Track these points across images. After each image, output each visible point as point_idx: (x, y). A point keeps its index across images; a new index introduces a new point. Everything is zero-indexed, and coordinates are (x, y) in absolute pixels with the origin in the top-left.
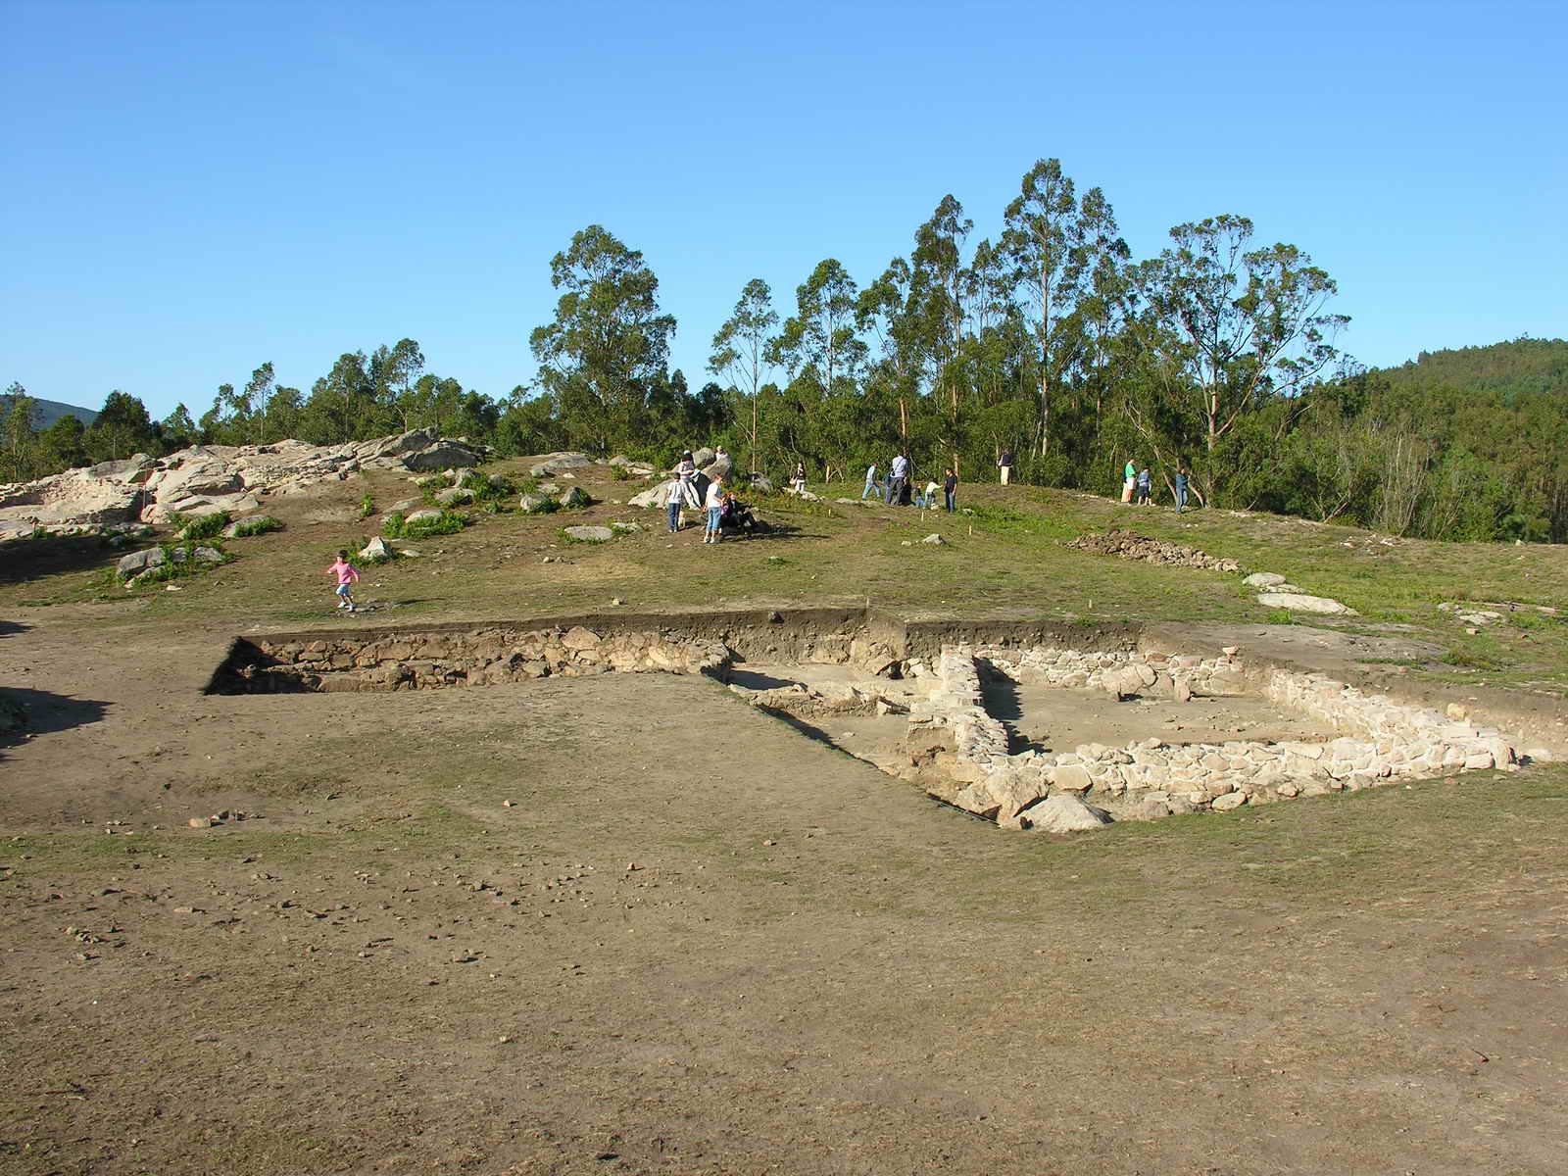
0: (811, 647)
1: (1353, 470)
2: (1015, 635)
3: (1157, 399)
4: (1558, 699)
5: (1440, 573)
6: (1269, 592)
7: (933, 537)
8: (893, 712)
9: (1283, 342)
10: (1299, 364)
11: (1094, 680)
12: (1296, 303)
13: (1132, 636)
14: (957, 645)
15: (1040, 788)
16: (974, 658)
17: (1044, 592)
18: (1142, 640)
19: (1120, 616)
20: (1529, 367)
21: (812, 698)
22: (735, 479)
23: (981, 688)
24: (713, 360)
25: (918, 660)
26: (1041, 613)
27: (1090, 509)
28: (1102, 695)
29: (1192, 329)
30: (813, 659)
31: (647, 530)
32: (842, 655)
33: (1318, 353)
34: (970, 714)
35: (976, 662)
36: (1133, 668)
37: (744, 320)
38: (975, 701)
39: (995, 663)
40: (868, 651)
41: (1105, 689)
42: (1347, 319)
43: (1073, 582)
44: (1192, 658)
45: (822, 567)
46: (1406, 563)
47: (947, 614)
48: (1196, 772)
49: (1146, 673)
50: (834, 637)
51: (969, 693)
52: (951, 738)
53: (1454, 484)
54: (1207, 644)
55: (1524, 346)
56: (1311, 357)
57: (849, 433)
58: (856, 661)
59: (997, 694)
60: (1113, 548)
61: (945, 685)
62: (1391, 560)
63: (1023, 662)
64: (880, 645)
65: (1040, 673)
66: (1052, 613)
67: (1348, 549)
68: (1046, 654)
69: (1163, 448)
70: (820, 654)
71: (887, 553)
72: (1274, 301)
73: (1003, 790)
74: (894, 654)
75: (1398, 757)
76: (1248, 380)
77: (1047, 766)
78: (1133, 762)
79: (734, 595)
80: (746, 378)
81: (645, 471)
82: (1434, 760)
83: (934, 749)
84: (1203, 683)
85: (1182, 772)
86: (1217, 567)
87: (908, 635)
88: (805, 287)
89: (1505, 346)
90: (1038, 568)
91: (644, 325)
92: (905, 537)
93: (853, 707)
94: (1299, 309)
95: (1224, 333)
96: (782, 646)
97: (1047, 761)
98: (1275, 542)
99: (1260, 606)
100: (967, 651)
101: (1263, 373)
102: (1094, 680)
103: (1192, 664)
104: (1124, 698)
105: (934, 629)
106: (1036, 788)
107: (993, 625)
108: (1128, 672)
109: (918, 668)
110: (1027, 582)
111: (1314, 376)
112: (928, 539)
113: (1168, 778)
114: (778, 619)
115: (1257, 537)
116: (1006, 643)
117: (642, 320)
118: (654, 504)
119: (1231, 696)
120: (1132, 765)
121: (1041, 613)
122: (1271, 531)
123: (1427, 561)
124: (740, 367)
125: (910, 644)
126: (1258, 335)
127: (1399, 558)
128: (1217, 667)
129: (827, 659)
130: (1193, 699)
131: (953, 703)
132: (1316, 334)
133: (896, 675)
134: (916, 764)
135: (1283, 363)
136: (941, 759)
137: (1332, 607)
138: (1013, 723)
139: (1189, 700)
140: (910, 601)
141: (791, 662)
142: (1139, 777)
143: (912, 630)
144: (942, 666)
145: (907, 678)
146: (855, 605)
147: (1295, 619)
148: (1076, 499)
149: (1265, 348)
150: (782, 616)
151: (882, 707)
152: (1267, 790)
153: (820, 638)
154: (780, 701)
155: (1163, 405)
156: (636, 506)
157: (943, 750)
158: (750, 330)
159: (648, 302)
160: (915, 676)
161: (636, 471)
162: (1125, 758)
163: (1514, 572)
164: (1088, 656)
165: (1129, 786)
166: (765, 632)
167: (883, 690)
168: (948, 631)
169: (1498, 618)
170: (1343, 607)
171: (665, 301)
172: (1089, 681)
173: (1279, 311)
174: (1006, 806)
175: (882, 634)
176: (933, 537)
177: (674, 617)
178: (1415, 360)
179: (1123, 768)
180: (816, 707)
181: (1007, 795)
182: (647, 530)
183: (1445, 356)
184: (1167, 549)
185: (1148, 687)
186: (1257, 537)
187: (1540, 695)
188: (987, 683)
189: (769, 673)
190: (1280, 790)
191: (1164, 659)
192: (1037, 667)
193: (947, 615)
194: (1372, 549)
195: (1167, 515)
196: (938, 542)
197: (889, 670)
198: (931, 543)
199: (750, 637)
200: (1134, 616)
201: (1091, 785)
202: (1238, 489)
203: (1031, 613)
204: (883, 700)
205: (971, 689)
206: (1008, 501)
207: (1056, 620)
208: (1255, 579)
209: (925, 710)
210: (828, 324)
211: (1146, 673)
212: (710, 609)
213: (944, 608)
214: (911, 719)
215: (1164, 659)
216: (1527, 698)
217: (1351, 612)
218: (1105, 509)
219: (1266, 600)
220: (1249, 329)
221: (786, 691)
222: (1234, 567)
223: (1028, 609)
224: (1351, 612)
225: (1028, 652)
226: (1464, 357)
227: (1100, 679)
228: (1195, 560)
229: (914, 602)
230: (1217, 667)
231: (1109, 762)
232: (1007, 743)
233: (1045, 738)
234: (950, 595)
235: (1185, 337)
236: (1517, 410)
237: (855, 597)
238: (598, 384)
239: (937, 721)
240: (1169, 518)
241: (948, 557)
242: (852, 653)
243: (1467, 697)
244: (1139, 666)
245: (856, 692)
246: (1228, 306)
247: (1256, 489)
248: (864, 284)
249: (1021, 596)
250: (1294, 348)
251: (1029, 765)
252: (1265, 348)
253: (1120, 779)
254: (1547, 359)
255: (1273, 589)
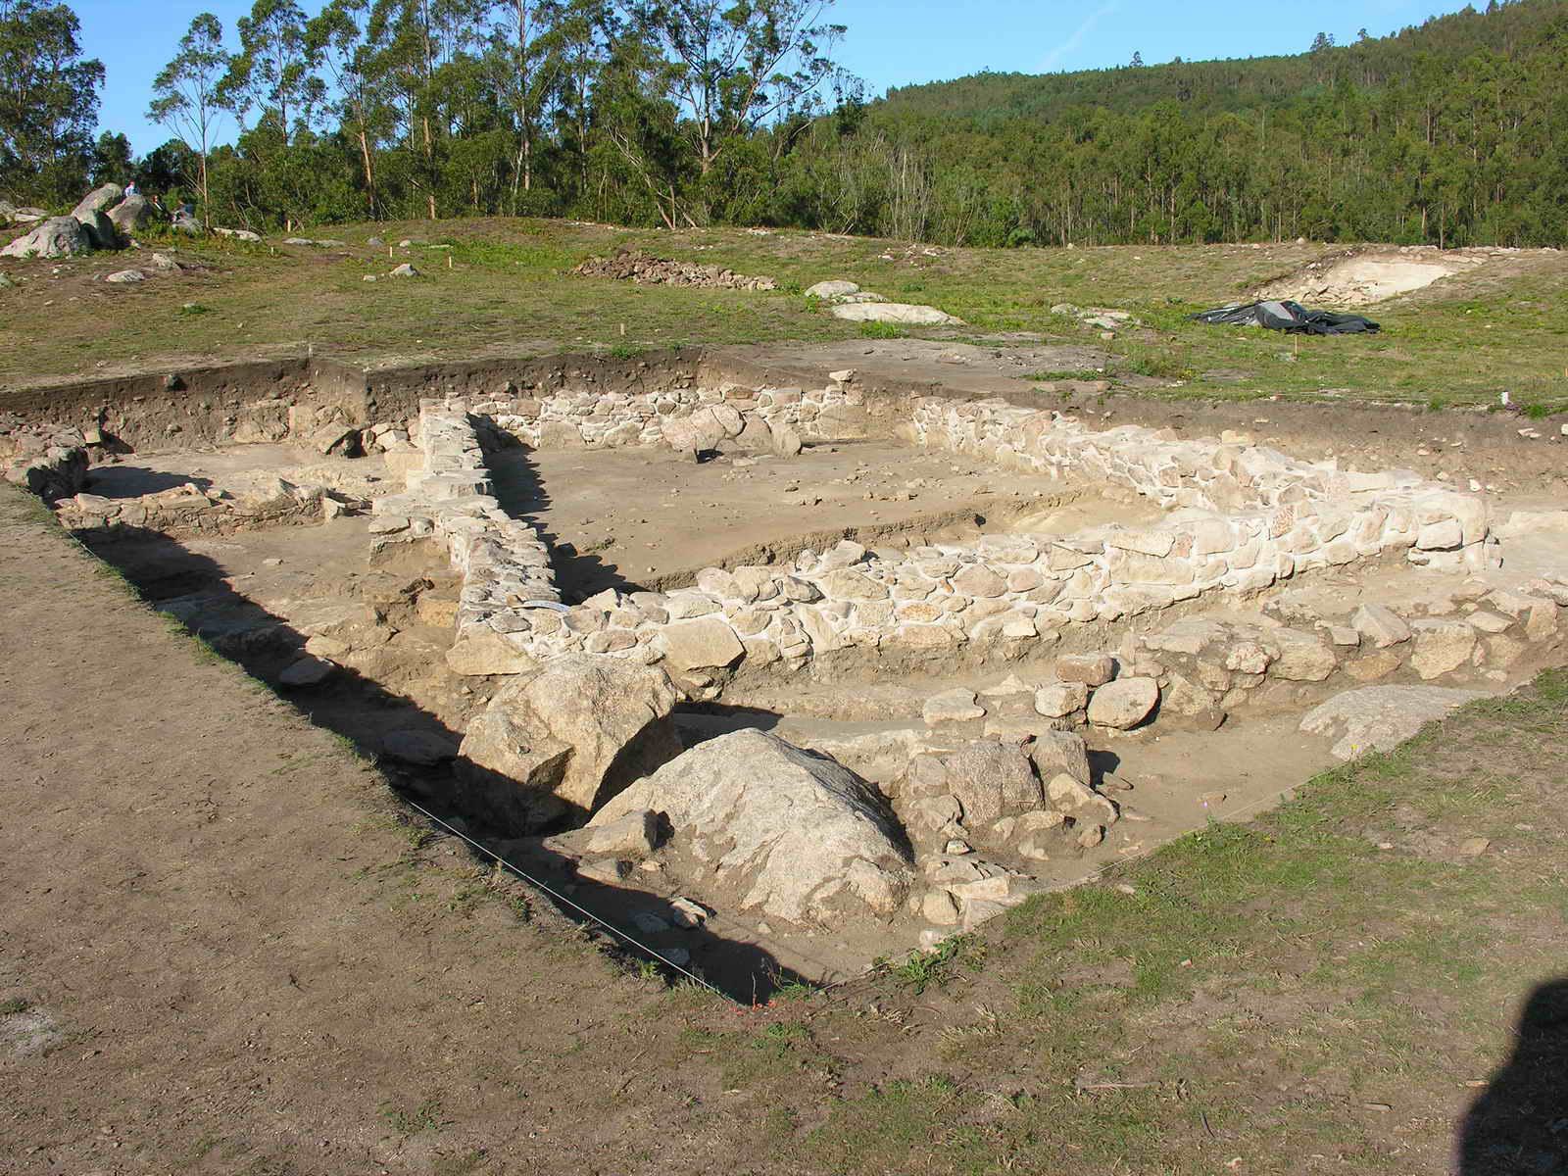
0: (233, 421)
1: (859, 189)
2: (525, 379)
3: (644, 121)
4: (1418, 413)
5: (997, 283)
6: (845, 302)
7: (404, 268)
8: (349, 512)
9: (778, 55)
10: (794, 80)
11: (649, 433)
12: (791, 13)
13: (688, 366)
14: (443, 397)
15: (656, 695)
16: (469, 416)
17: (554, 320)
18: (703, 372)
19: (668, 341)
20: (991, 100)
21: (214, 502)
22: (150, 220)
23: (487, 462)
24: (155, 105)
25: (386, 426)
26: (559, 345)
27: (586, 238)
28: (666, 455)
29: (680, 45)
30: (238, 438)
31: (19, 285)
32: (279, 428)
33: (814, 67)
34: (474, 514)
35: (473, 421)
36: (708, 411)
37: (190, 59)
38: (479, 487)
39: (502, 420)
40: (315, 419)
41: (670, 445)
42: (842, 29)
43: (592, 307)
44: (789, 391)
45: (253, 314)
46: (957, 273)
47: (425, 356)
48: (947, 604)
49: (728, 416)
50: (264, 403)
51: (467, 475)
52: (444, 559)
53: (962, 200)
54: (802, 369)
55: (984, 79)
56: (806, 72)
57: (309, 181)
58: (298, 435)
59: (511, 476)
60: (625, 272)
61: (427, 462)
62: (939, 271)
63: (543, 415)
64: (330, 409)
65: (569, 429)
66: (572, 343)
67: (887, 262)
68: (578, 401)
69: (653, 175)
70: (247, 430)
71: (342, 290)
72: (767, 12)
73: (574, 711)
74: (352, 420)
75: (1305, 540)
76: (742, 98)
77: (649, 625)
78: (822, 597)
79: (125, 355)
80: (193, 125)
81: (32, 218)
82: (1367, 538)
83: (413, 588)
84: (808, 425)
85: (917, 607)
86: (750, 286)
87: (370, 390)
88: (247, 20)
89: (968, 80)
90: (542, 295)
91: (67, 71)
92: (366, 271)
93: (283, 511)
94: (795, 18)
95: (715, 50)
96: (189, 422)
97: (649, 615)
98: (805, 259)
99: (837, 320)
100: (458, 406)
101: (758, 90)
102: (649, 433)
103: (790, 399)
104: (705, 456)
105: (407, 378)
106: (648, 696)
107: (492, 366)
108: (701, 418)
109: (388, 439)
110: (530, 310)
111: (811, 92)
112: (397, 271)
113: (892, 622)
114: (179, 385)
115: (783, 254)
116: (513, 390)
117: (61, 68)
118: (34, 253)
119: (847, 442)
120: (819, 605)
121: (559, 345)
122: (797, 248)
123: (978, 270)
124: (186, 114)
125: (374, 403)
126: (750, 48)
127: (947, 268)
128: (826, 401)
129: (257, 437)
130: (805, 449)
131: (443, 494)
132: (810, 45)
133: (356, 452)
134: (382, 619)
135: (777, 79)
136: (429, 607)
137: (931, 315)
138: (542, 517)
139: (799, 452)
140: (371, 345)
141: (205, 445)
142: (835, 626)
143: (374, 383)
144: (423, 432)
145: (373, 455)
146: (293, 356)
147: (918, 332)
148: (568, 228)
149: (758, 64)
150: (185, 379)
151: (330, 506)
152: (1200, 663)
153: (246, 406)
154: (161, 514)
155: (651, 129)
156: (10, 257)
157: (431, 586)
158: (195, 70)
159: (72, 47)
160: (384, 450)
161: (19, 218)
162: (806, 592)
163: (1079, 277)
164: (638, 398)
165: (819, 647)
166: (162, 405)
167: (335, 476)
168: (428, 380)
169: (1130, 319)
170: (945, 316)
171: (90, 45)
172: (643, 435)
173: (772, 22)
174: (585, 749)
175: (333, 392)
176: (404, 268)
177: (21, 395)
178: (883, 96)
179: (801, 612)
180: (223, 517)
181: (585, 721)
182: (19, 285)
183: (911, 93)
184: (688, 269)
185: (733, 438)
186: (783, 254)
187: (1383, 410)
188: (493, 451)
189: (159, 466)
190: (1232, 663)
191: (750, 395)
192: (565, 422)
193: (425, 358)
194: (915, 261)
195: (676, 237)
196: (409, 273)
197: (345, 445)
198: (401, 275)
199: (139, 413)
200: (687, 341)
201: (742, 656)
202: (737, 216)
203: (544, 346)
204: (333, 495)
205: (471, 468)
206: (492, 235)
207: (584, 353)
208: (822, 289)
209: (395, 510)
210: (282, 58)
211: (728, 416)
212: (77, 378)
213: (420, 349)
214: (373, 528)
215: (750, 395)
216: (1359, 415)
217: (955, 320)
218: (606, 237)
219: (845, 313)
220: (740, 44)
221: (171, 497)
222: (770, 286)
223: (538, 342)
224: (955, 320)
225: (548, 399)
226: (930, 91)
227: (660, 431)
228: (724, 280)
229: (377, 345)
230: (826, 400)
231: (773, 603)
232: (551, 573)
233: (609, 543)
234: (429, 333)
235: (674, 57)
236: (992, 135)
237: (293, 345)
238: (17, 144)
239: (418, 527)
240: (679, 241)
241: (423, 290)
242: (292, 424)
243: (1251, 420)
244: (717, 409)
245: (286, 485)
246: (716, 18)
247: (756, 214)
248: (314, 13)
249: (526, 326)
250: (789, 63)
251: (611, 626)
252: (758, 64)
253: (798, 636)
254: (1008, 92)
255: (850, 299)
